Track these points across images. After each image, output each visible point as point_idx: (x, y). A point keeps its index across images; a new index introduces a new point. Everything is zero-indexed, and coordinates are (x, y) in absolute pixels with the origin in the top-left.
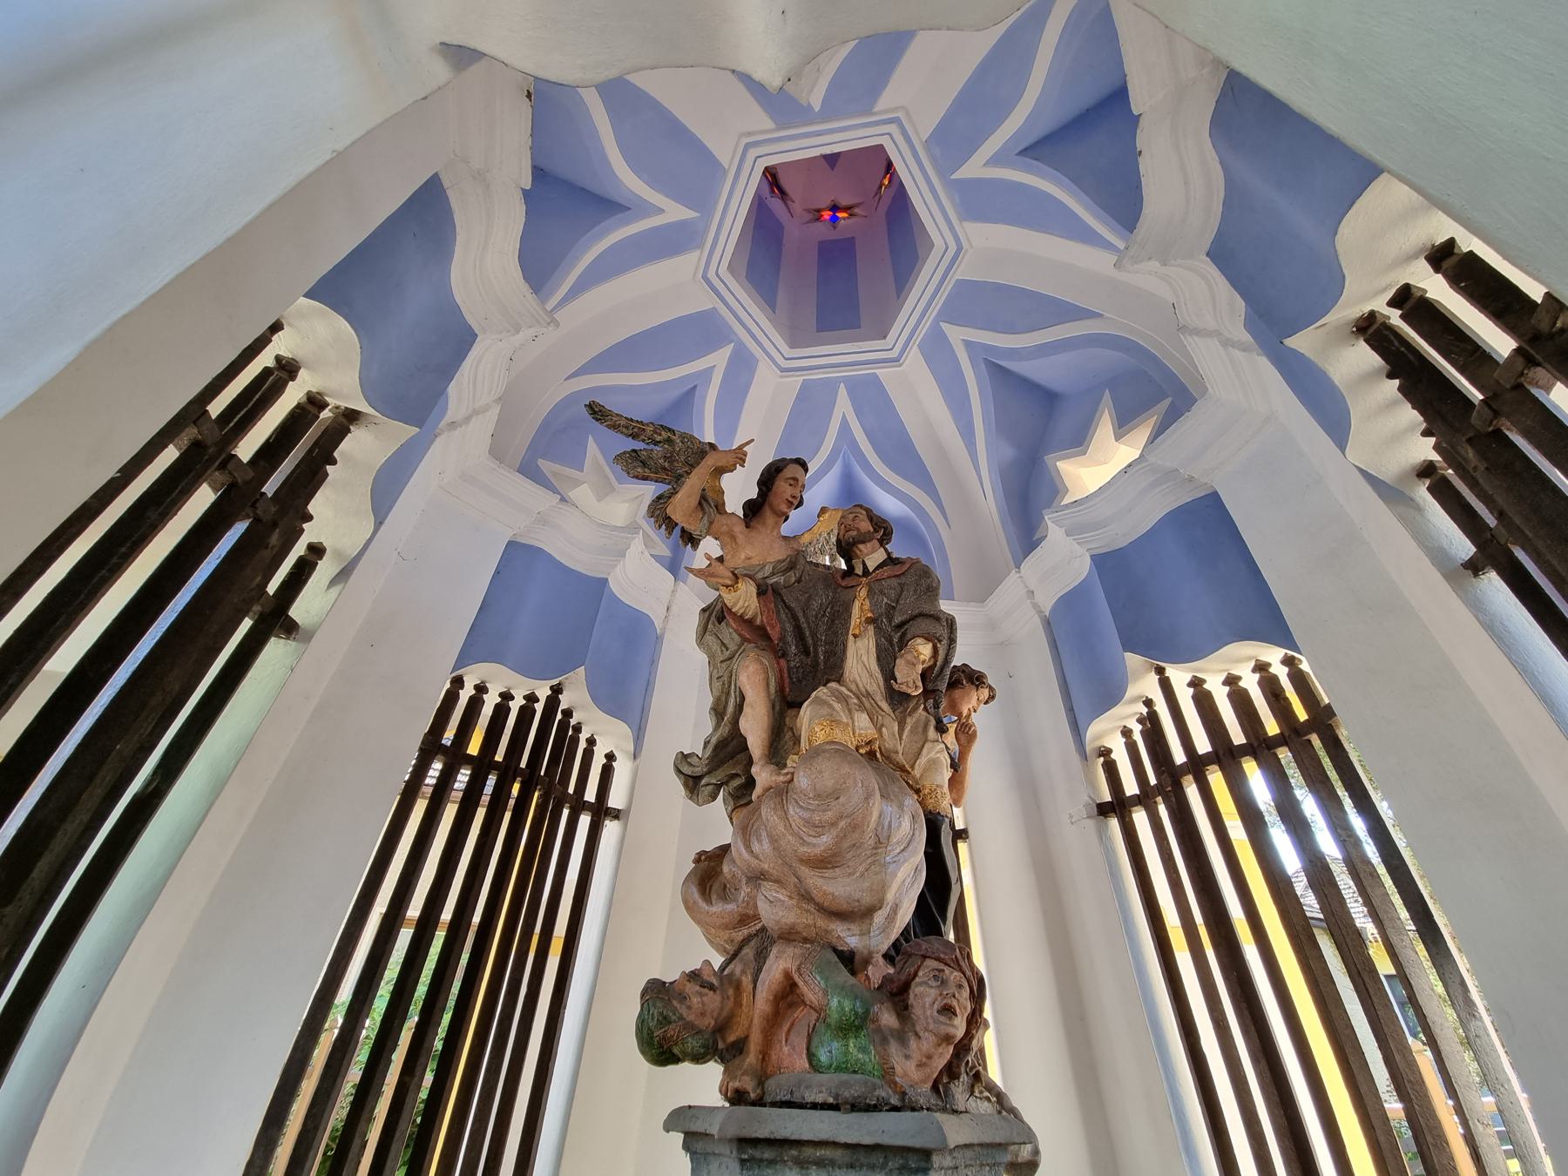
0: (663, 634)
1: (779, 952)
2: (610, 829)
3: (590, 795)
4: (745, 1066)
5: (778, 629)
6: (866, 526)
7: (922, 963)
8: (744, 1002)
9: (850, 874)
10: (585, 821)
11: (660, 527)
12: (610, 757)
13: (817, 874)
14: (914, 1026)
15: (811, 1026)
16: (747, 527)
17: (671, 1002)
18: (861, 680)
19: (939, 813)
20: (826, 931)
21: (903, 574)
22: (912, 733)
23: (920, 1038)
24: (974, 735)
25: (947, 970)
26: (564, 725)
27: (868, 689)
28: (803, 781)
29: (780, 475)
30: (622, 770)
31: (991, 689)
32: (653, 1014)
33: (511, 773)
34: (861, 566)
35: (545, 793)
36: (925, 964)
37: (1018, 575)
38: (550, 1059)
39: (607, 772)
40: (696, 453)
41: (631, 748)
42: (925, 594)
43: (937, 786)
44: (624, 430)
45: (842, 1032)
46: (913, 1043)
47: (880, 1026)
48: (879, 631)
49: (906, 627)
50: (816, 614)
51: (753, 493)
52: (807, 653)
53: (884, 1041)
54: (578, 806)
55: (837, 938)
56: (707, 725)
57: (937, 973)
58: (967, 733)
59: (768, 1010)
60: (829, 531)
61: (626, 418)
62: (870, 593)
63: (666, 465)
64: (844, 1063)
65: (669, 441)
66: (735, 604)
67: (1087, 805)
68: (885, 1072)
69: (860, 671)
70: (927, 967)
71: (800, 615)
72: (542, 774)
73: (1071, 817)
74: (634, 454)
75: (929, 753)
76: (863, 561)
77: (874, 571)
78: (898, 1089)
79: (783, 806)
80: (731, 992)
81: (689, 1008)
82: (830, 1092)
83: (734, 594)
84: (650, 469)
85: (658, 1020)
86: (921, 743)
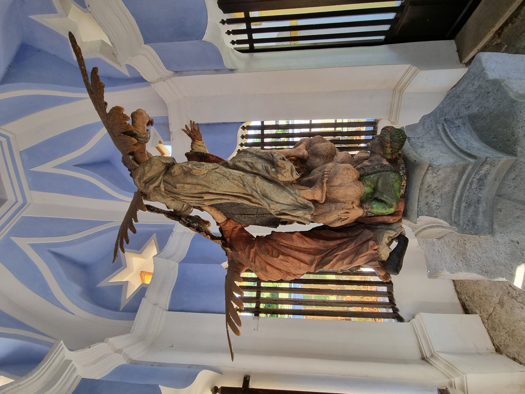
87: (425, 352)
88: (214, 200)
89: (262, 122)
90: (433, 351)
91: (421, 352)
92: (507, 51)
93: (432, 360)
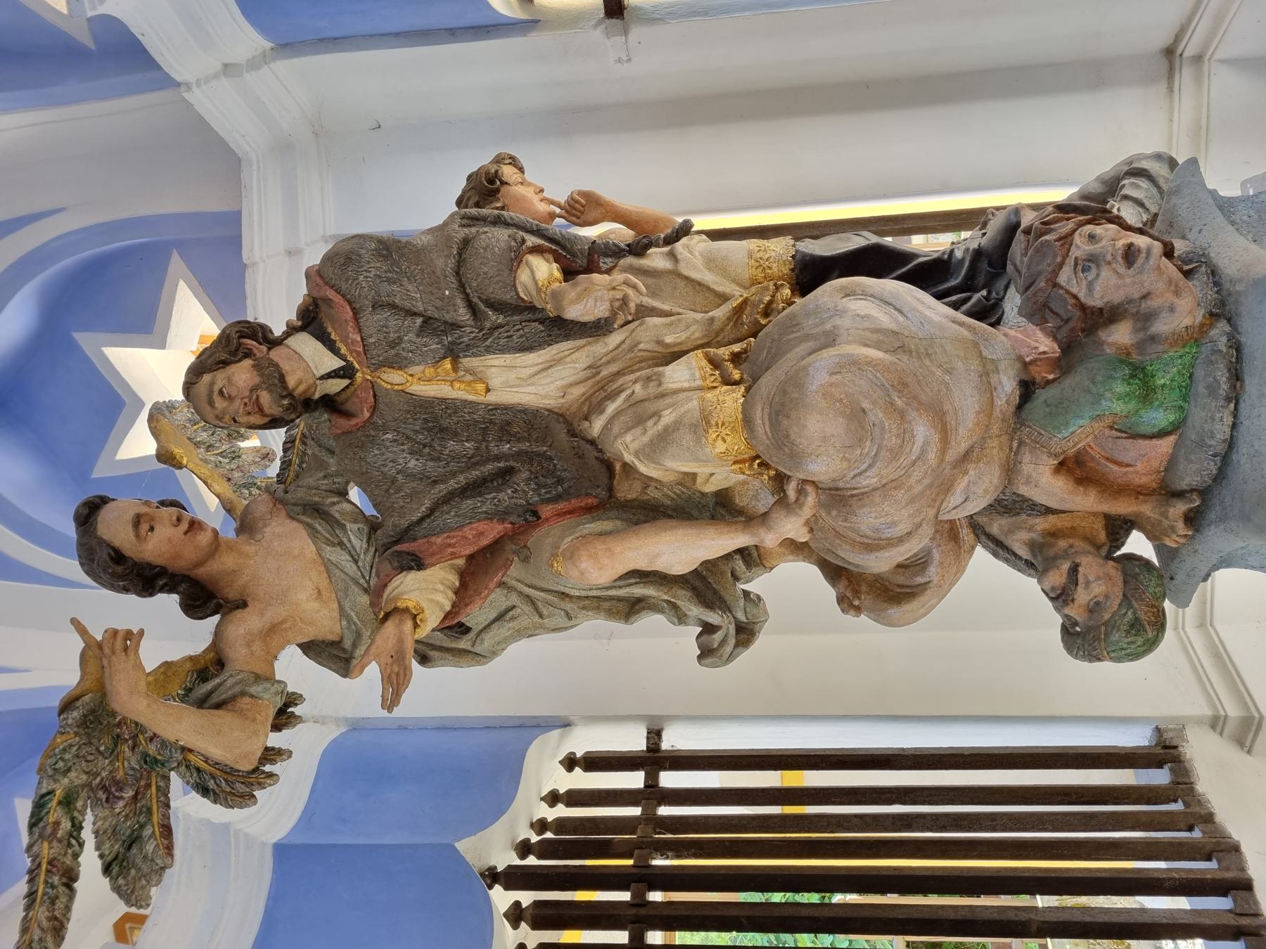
0: (346, 720)
1: (1027, 482)
2: (676, 739)
3: (634, 780)
4: (1156, 517)
5: (482, 526)
6: (242, 375)
7: (1062, 288)
8: (1068, 524)
9: (947, 389)
10: (670, 779)
11: (271, 775)
12: (570, 763)
13: (953, 437)
14: (1130, 301)
15: (1119, 434)
16: (243, 605)
17: (1109, 620)
18: (563, 379)
19: (793, 257)
20: (1003, 420)
21: (349, 303)
22: (657, 295)
23: (1149, 294)
24: (588, 196)
25: (1075, 253)
26: (545, 850)
27: (584, 366)
28: (822, 467)
29: (127, 553)
30: (586, 741)
31: (499, 160)
32: (1128, 643)
33: (643, 911)
34: (330, 381)
35: (656, 850)
36: (1063, 284)
37: (195, 89)
38: (962, 755)
39: (594, 762)
40: (88, 735)
41: (556, 733)
42: (395, 263)
43: (750, 257)
44: (60, 904)
45: (1149, 394)
46: (1153, 303)
47: (1132, 345)
48: (471, 349)
49: (475, 300)
50: (432, 459)
51: (168, 602)
52: (510, 471)
53: (1153, 339)
54: (653, 794)
55: (1008, 404)
56: (653, 622)
57: (1080, 267)
58: (583, 206)
59: (1094, 492)
60: (192, 446)
61: (28, 908)
62: (397, 363)
63: (129, 793)
64: (1181, 391)
65: (68, 802)
66: (441, 606)
67: (608, 34)
68: (1191, 339)
69: (549, 380)
70: (1069, 280)
71: (442, 489)
72: (630, 862)
73: (620, 61)
74: (115, 869)
75: (695, 268)
76: (322, 378)
77: (343, 358)
78: (1207, 322)
79: (863, 494)
80: (1062, 544)
81: (1107, 597)
82: (1222, 407)
83: (427, 612)
84: (142, 827)
85: (1135, 635)
86: (679, 280)
87: (1197, 25)
88: (473, 655)
89: (655, 735)
90: (1210, 52)
91: (1178, 38)
92: (1225, 567)
93: (1185, 76)
